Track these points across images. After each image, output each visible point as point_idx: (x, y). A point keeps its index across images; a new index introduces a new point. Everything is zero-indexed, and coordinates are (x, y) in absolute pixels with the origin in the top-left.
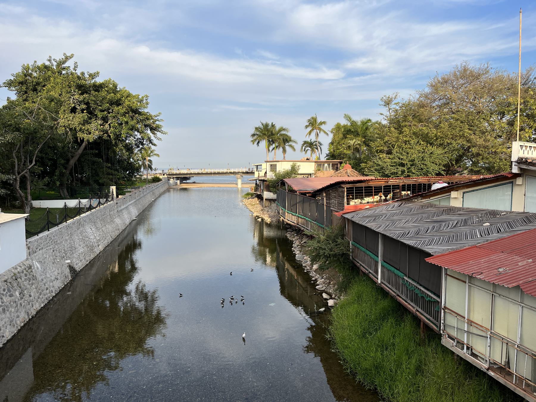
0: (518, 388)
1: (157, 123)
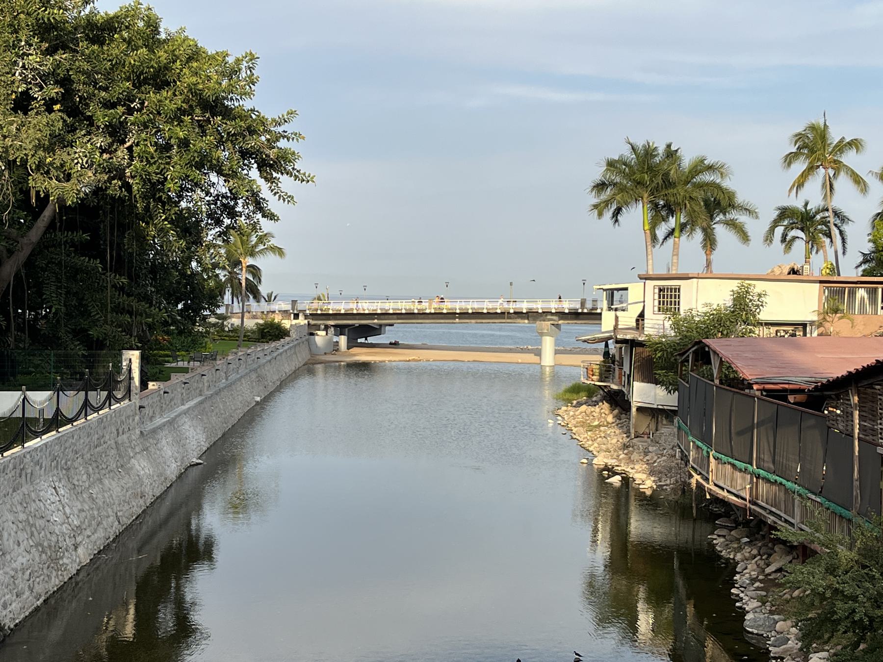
1: (282, 144)
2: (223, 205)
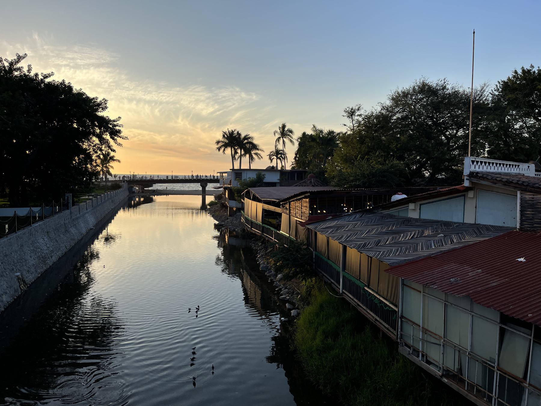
0: (470, 395)
1: (117, 128)
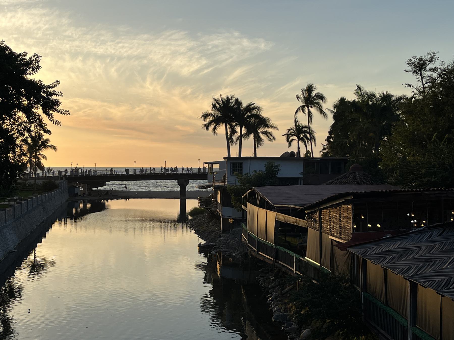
1: (54, 97)
2: (25, 127)
